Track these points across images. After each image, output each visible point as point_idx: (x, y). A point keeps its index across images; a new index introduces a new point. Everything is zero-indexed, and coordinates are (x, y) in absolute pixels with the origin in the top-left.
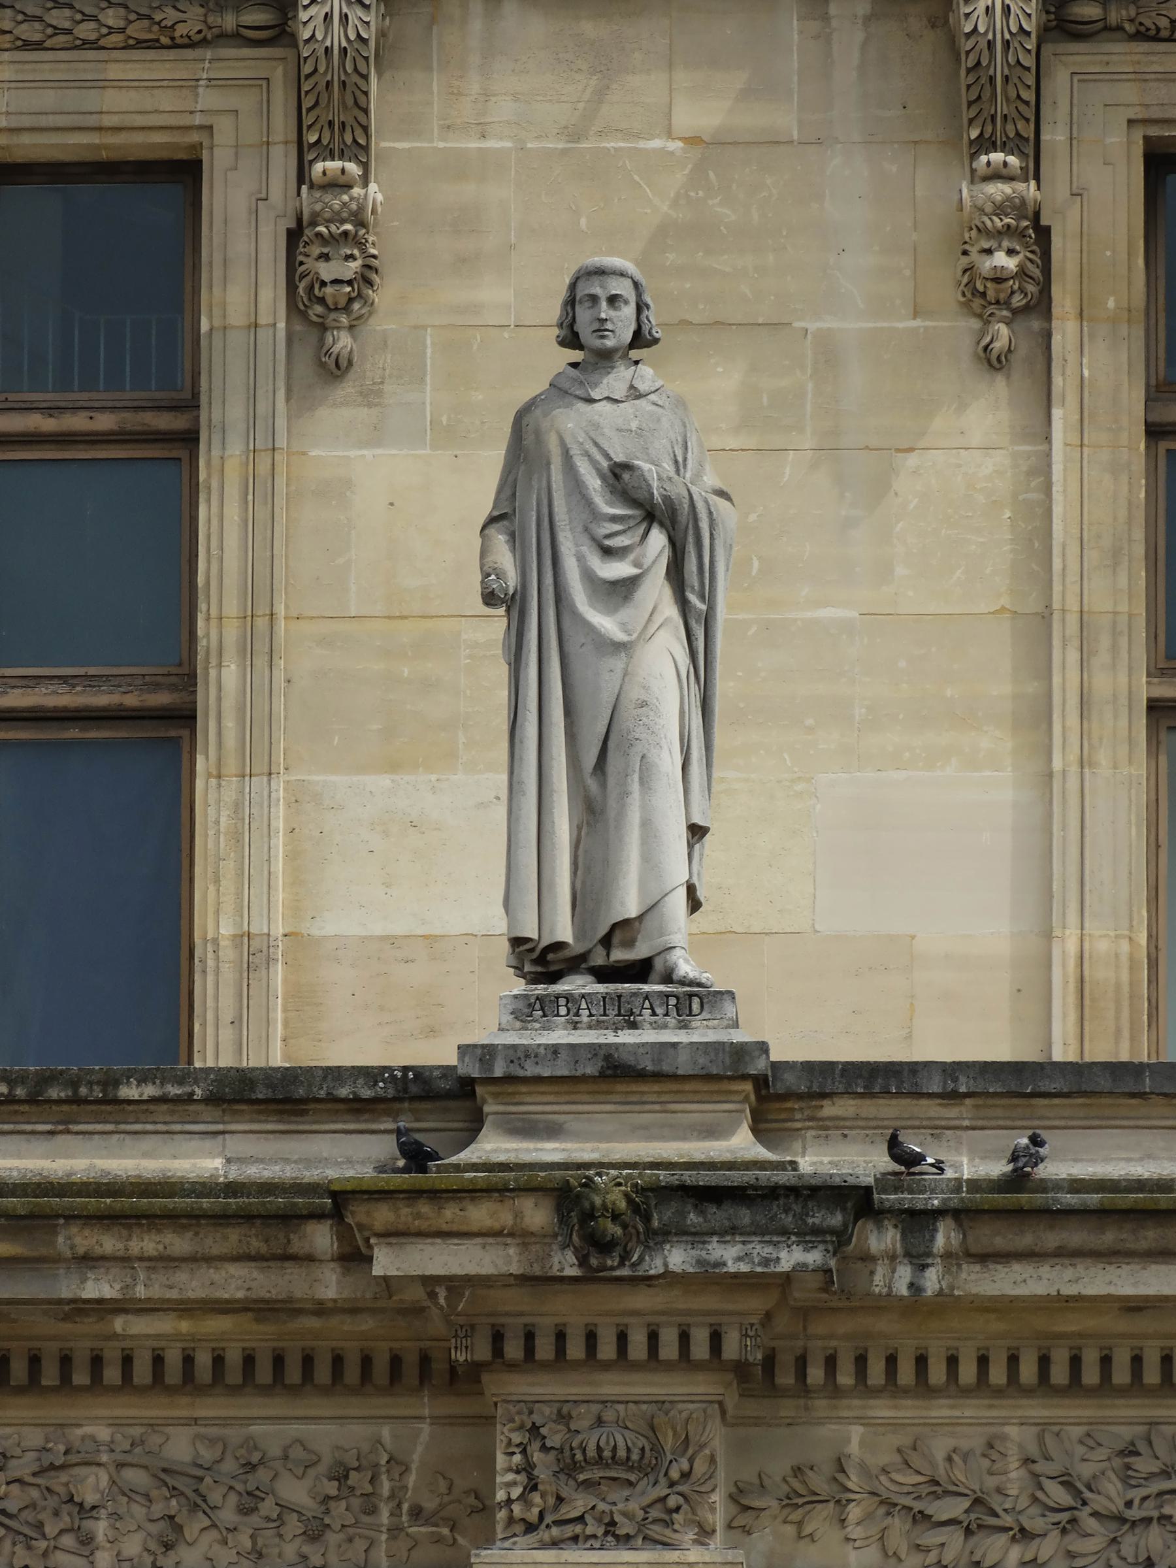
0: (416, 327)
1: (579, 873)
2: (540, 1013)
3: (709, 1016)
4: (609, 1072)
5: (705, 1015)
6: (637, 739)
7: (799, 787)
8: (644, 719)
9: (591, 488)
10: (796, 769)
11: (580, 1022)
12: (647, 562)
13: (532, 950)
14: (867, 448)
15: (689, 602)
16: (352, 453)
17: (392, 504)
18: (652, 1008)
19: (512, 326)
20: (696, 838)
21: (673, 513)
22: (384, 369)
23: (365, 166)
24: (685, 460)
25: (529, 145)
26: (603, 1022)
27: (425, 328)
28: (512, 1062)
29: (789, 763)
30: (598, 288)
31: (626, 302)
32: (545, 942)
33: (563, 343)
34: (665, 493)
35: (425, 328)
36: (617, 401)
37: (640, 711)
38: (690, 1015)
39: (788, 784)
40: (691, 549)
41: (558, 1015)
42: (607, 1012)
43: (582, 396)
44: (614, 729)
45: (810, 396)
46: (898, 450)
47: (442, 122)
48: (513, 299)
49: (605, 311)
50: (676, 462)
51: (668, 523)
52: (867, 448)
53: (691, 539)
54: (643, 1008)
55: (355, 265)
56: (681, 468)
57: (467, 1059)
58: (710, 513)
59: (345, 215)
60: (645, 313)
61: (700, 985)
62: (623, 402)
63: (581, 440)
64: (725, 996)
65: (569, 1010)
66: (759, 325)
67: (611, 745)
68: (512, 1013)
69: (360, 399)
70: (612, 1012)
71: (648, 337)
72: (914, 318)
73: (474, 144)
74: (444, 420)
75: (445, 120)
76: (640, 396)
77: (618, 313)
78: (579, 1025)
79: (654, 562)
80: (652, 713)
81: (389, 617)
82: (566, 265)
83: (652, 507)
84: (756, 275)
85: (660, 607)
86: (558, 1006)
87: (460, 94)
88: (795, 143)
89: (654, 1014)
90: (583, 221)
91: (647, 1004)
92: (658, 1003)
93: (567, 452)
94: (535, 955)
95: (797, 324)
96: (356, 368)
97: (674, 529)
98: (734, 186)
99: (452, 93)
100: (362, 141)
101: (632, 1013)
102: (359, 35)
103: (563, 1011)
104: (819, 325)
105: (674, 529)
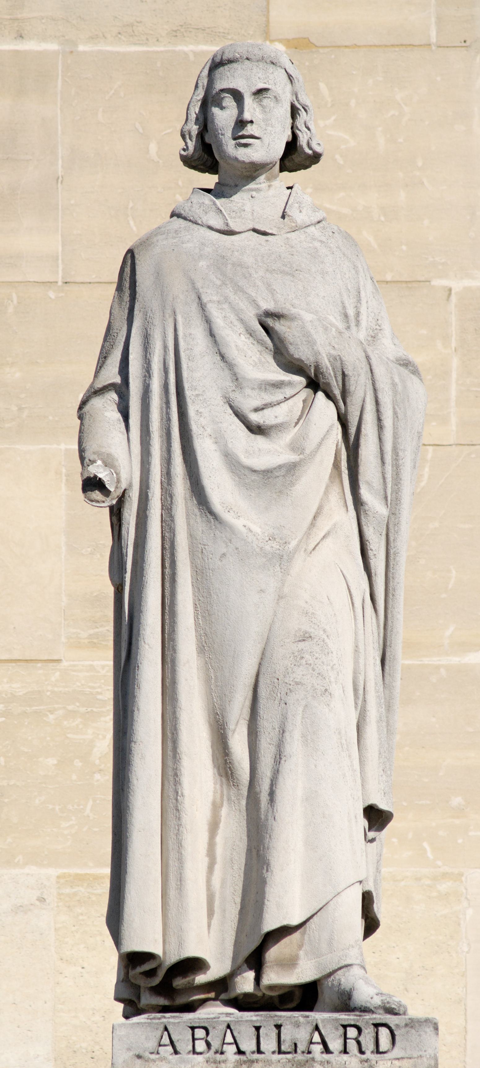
5: (397, 1052)
6: (297, 683)
7: (444, 887)
8: (307, 656)
10: (439, 863)
12: (310, 446)
13: (151, 973)
19: (60, 283)
24: (358, 314)
25: (81, 48)
29: (430, 855)
32: (172, 958)
33: (188, 162)
34: (333, 352)
37: (301, 645)
39: (428, 882)
40: (369, 430)
42: (263, 1048)
43: (218, 227)
45: (454, 375)
48: (60, 249)
50: (346, 316)
54: (311, 1043)
56: (353, 324)
65: (208, 1045)
66: (387, 282)
67: (263, 692)
79: (320, 444)
82: (131, 205)
84: (382, 218)
85: (326, 509)
88: (434, 48)
89: (327, 1050)
90: (153, 147)
91: (316, 1038)
93: (199, 298)
94: (156, 981)
95: (437, 282)
97: (345, 403)
98: (353, 103)
104: (467, 283)
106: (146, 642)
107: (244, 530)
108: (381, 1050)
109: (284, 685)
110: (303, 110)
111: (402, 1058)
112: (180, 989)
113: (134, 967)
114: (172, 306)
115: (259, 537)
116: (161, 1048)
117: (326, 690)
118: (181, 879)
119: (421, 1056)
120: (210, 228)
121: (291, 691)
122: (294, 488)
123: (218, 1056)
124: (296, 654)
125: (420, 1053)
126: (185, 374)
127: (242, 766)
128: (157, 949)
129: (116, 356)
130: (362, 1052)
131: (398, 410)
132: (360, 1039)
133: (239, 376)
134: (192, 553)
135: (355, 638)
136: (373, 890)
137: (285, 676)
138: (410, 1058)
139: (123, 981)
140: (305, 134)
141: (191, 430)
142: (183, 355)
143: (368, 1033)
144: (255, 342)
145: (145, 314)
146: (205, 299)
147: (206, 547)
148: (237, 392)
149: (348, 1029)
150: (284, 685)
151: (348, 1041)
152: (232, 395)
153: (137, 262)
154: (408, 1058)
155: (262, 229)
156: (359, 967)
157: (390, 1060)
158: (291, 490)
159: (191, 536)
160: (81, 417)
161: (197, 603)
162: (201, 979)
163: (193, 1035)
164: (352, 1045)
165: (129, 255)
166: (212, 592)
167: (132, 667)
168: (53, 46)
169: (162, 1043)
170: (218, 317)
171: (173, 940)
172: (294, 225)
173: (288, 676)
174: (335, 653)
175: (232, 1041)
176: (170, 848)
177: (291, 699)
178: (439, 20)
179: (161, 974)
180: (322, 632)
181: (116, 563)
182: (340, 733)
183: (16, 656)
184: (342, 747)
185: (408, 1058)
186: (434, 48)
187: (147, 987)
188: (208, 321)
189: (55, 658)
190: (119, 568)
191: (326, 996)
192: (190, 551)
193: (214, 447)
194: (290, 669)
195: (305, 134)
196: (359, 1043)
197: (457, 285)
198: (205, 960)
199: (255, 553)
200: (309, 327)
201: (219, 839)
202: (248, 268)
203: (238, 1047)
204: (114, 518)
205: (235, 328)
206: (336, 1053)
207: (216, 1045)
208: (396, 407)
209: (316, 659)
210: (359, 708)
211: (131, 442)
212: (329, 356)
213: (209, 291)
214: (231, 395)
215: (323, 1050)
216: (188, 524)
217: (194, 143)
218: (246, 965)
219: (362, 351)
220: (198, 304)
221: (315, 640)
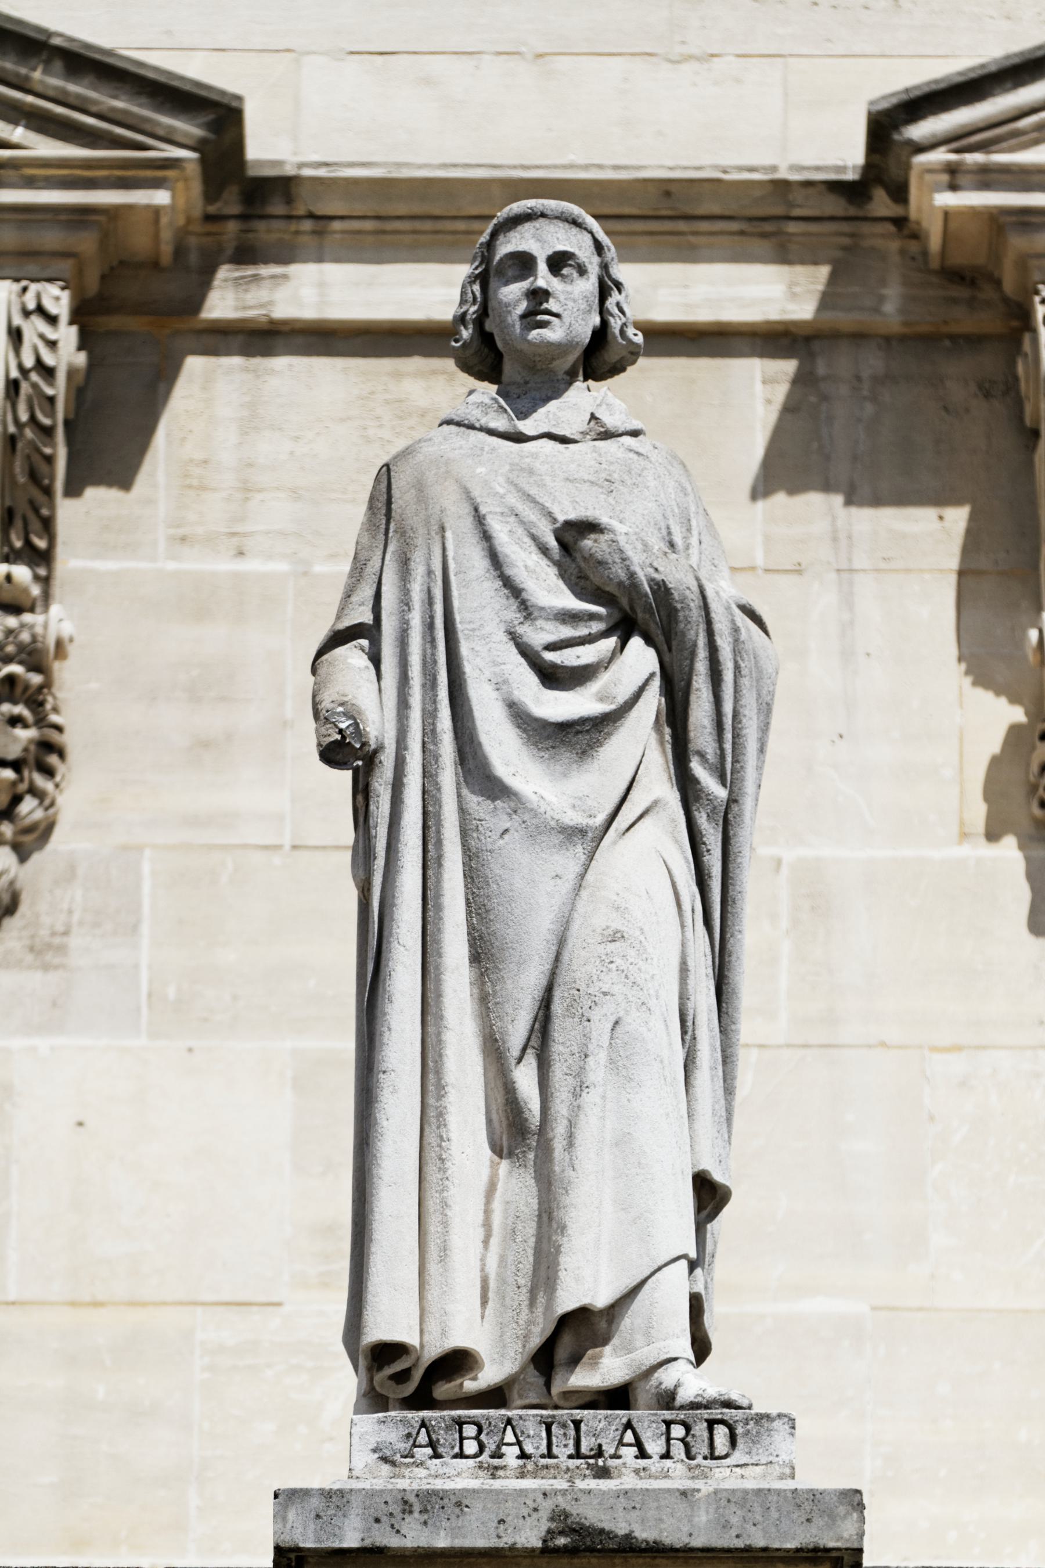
0: (125, 848)
1: (494, 1241)
2: (429, 1451)
3: (745, 1459)
4: (562, 1541)
5: (737, 1457)
6: (605, 994)
8: (619, 961)
9: (520, 564)
11: (503, 1468)
13: (402, 1377)
14: (883, 1044)
15: (697, 782)
16: (17, 1043)
17: (80, 1124)
18: (639, 1444)
19: (287, 847)
20: (705, 1213)
21: (669, 616)
22: (70, 912)
23: (46, 582)
26: (547, 1467)
27: (140, 849)
28: (377, 1520)
30: (532, 241)
31: (582, 271)
32: (433, 1351)
35: (140, 849)
36: (564, 440)
37: (611, 947)
38: (713, 1456)
40: (701, 684)
41: (461, 1455)
42: (555, 1450)
44: (562, 978)
46: (934, 1049)
47: (172, 531)
49: (543, 278)
51: (660, 639)
52: (883, 1044)
53: (701, 666)
55: (25, 735)
57: (291, 1515)
58: (736, 641)
59: (10, 649)
60: (615, 297)
61: (728, 1404)
62: (575, 441)
63: (501, 491)
64: (777, 1424)
65: (482, 1447)
67: (558, 1007)
68: (374, 1451)
69: (29, 958)
70: (563, 1451)
71: (620, 340)
72: (960, 843)
73: (225, 565)
74: (171, 992)
75: (178, 526)
76: (607, 435)
77: (569, 288)
78: (500, 1473)
80: (632, 953)
81: (73, 1304)
83: (631, 601)
86: (462, 1439)
87: (203, 488)
89: (643, 1454)
91: (629, 1437)
92: (649, 1434)
93: (476, 510)
96: (23, 908)
97: (670, 650)
99: (190, 487)
100: (41, 544)
101: (599, 1453)
102: (33, 418)
103: (471, 1447)
105: (670, 650)
106: (401, 942)
107: (534, 798)
108: (717, 1454)
109: (586, 997)
110: (615, 289)
111: (746, 1465)
112: (439, 1401)
113: (380, 1368)
114: (440, 520)
115: (554, 807)
116: (415, 1450)
117: (643, 1003)
118: (444, 1249)
119: (771, 1462)
120: (492, 432)
121: (596, 1004)
122: (602, 749)
123: (496, 1462)
124: (604, 957)
125: (771, 1458)
126: (456, 603)
127: (529, 1106)
128: (411, 1338)
129: (367, 592)
130: (690, 1456)
131: (740, 662)
132: (689, 1439)
133: (529, 604)
134: (464, 833)
135: (683, 951)
136: (703, 1293)
137: (588, 986)
138: (757, 1465)
139: (364, 1395)
140: (617, 319)
141: (464, 673)
142: (453, 579)
143: (700, 1429)
144: (551, 564)
145: (403, 534)
146: (483, 510)
147: (483, 822)
148: (527, 625)
149: (673, 1426)
150: (586, 997)
151: (672, 1442)
152: (520, 630)
153: (393, 480)
154: (752, 1464)
155: (561, 433)
156: (685, 1361)
157: (728, 1467)
158: (597, 751)
159: (462, 811)
160: (314, 671)
161: (470, 897)
162: (470, 1385)
163: (461, 1432)
164: (678, 1450)
165: (385, 469)
166: (490, 881)
167: (382, 978)
168: (281, 567)
169: (417, 1443)
170: (501, 531)
171: (433, 1326)
172: (602, 430)
173: (591, 985)
174: (655, 960)
175: (514, 1440)
176: (431, 1210)
177: (595, 1015)
178: (767, 539)
179: (417, 1375)
180: (638, 933)
181: (361, 851)
182: (662, 1062)
183: (226, 1297)
184: (665, 1080)
185: (752, 1464)
186: (760, 572)
187: (398, 1399)
188: (486, 537)
189: (275, 1299)
190: (365, 858)
191: (644, 1394)
192: (461, 830)
193: (495, 695)
194: (595, 978)
195: (617, 319)
196: (687, 1446)
197: (789, 855)
198: (478, 1353)
199: (548, 827)
200: (622, 541)
201: (497, 1205)
202: (541, 475)
203: (521, 1449)
204: (360, 798)
205: (524, 545)
206: (656, 1458)
207: (491, 1446)
208: (738, 659)
209: (631, 964)
210: (687, 1045)
211: (383, 692)
212: (651, 581)
213: (489, 501)
214: (517, 628)
215: (637, 1453)
216: (459, 795)
217: (470, 331)
218: (532, 1366)
219: (694, 579)
220: (474, 517)
221: (629, 941)
